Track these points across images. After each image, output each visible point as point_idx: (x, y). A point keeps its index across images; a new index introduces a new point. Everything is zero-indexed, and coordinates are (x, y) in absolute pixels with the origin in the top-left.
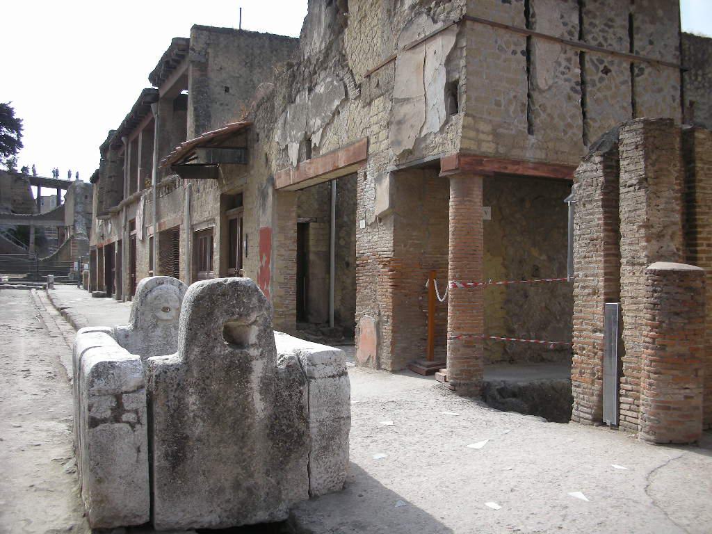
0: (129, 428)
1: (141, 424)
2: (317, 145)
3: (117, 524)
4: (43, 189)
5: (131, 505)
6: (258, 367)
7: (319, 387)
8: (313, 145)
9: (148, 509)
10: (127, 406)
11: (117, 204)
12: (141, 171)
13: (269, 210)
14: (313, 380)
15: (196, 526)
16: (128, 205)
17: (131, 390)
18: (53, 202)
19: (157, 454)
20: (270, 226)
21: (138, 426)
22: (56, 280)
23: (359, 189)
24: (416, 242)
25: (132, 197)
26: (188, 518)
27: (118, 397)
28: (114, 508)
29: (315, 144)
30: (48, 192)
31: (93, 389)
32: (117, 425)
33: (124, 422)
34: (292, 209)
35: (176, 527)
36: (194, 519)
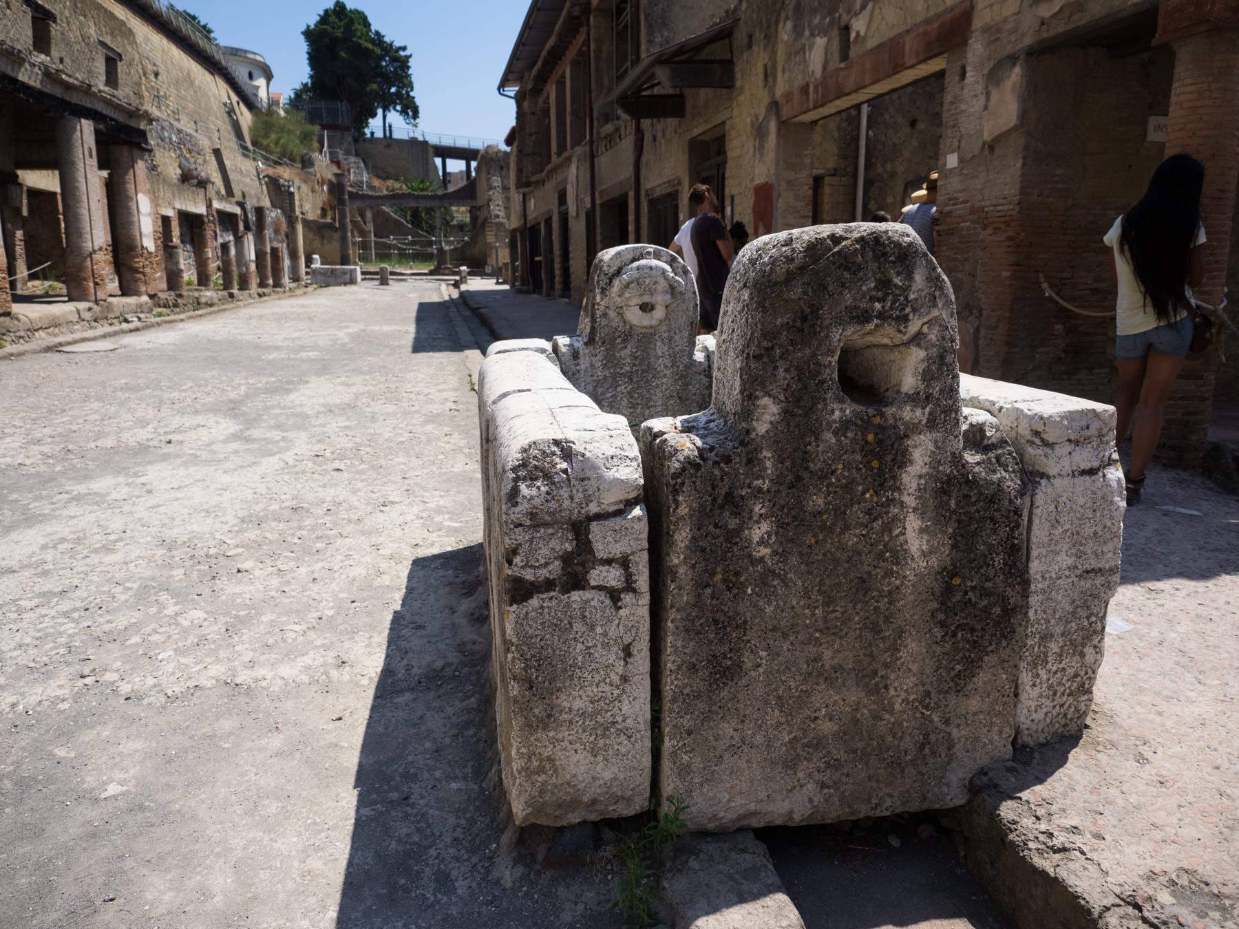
0: (608, 602)
1: (634, 591)
2: (862, 34)
3: (574, 818)
4: (449, 162)
5: (607, 775)
6: (921, 451)
7: (1056, 501)
8: (853, 36)
9: (647, 784)
10: (600, 549)
11: (541, 171)
12: (571, 121)
13: (770, 156)
14: (1043, 482)
15: (756, 823)
16: (554, 170)
17: (612, 509)
18: (462, 179)
19: (670, 662)
20: (772, 180)
21: (627, 598)
22: (469, 274)
23: (948, 98)
24: (1059, 186)
25: (560, 159)
26: (742, 805)
27: (580, 529)
28: (569, 784)
29: (858, 33)
30: (456, 166)
31: (516, 510)
32: (576, 596)
33: (593, 588)
34: (806, 152)
35: (711, 826)
36: (753, 807)
